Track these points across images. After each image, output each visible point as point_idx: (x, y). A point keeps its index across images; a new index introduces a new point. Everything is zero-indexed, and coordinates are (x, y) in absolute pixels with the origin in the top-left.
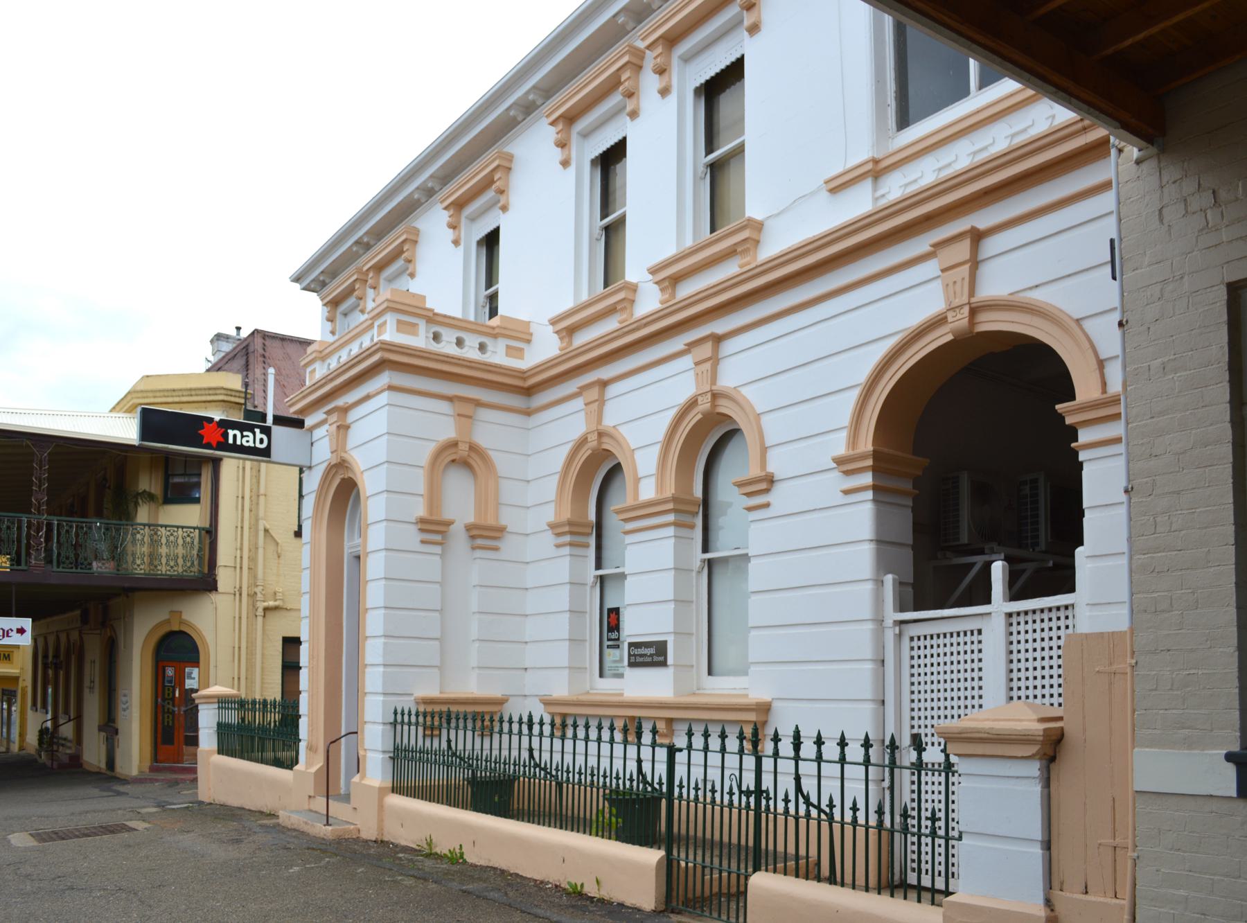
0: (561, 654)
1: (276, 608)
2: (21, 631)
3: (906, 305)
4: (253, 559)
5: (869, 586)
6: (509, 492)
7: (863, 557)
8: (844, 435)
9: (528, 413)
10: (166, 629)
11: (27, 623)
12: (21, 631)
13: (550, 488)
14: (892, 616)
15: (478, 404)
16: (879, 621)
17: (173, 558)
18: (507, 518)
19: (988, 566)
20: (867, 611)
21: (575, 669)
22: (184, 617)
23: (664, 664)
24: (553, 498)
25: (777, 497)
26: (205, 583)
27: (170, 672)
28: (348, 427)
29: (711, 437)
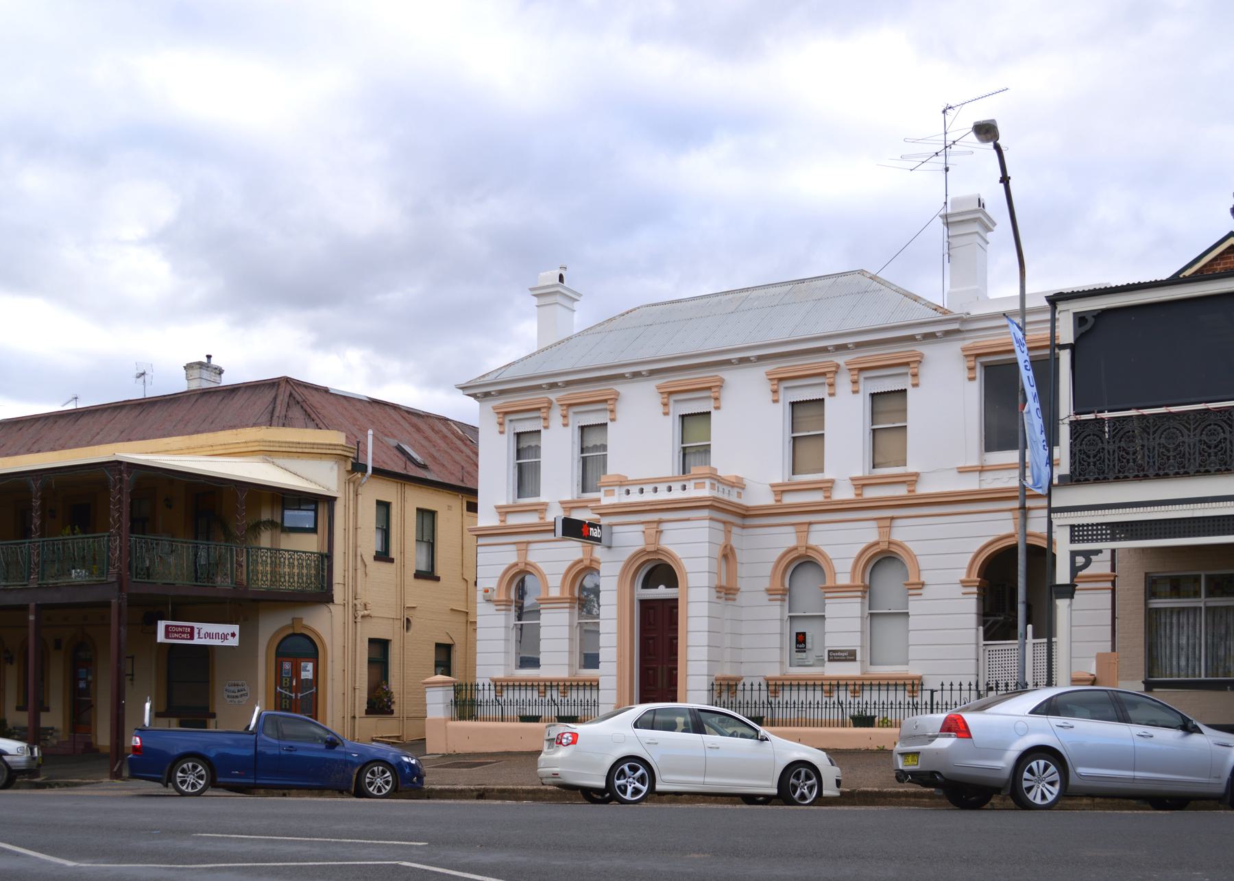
0: (776, 656)
1: (368, 615)
2: (233, 635)
3: (998, 526)
4: (355, 578)
5: (974, 631)
6: (742, 571)
7: (972, 619)
8: (965, 571)
9: (744, 527)
10: (290, 631)
11: (235, 628)
12: (233, 635)
13: (769, 568)
14: (982, 642)
15: (733, 524)
16: (977, 644)
17: (293, 577)
18: (742, 584)
19: (338, 428)
20: (974, 641)
21: (570, 665)
22: (305, 622)
23: (855, 660)
24: (769, 573)
25: (925, 591)
26: (325, 597)
27: (287, 666)
28: (661, 532)
29: (882, 559)
